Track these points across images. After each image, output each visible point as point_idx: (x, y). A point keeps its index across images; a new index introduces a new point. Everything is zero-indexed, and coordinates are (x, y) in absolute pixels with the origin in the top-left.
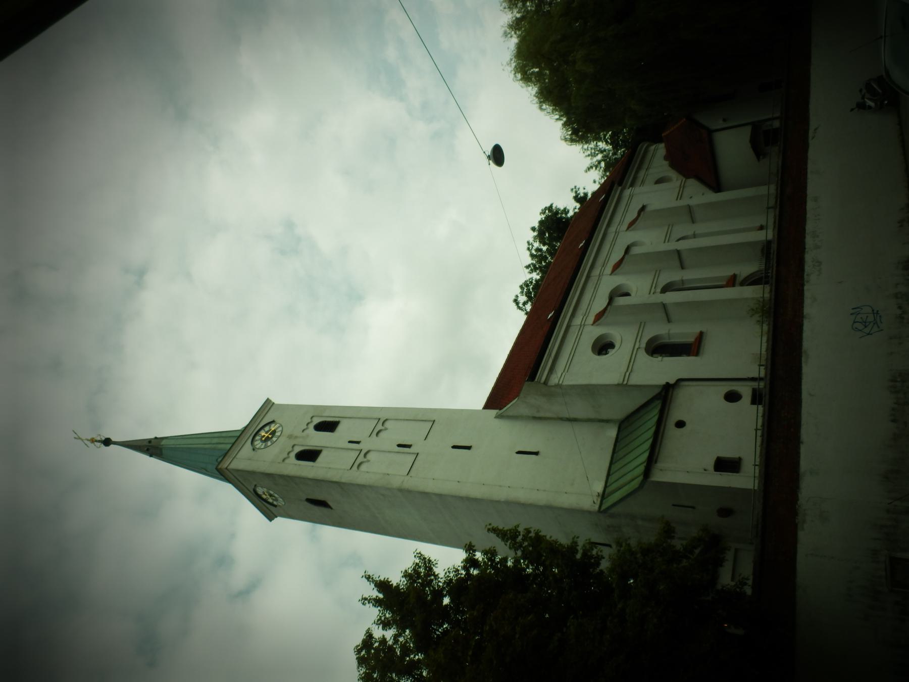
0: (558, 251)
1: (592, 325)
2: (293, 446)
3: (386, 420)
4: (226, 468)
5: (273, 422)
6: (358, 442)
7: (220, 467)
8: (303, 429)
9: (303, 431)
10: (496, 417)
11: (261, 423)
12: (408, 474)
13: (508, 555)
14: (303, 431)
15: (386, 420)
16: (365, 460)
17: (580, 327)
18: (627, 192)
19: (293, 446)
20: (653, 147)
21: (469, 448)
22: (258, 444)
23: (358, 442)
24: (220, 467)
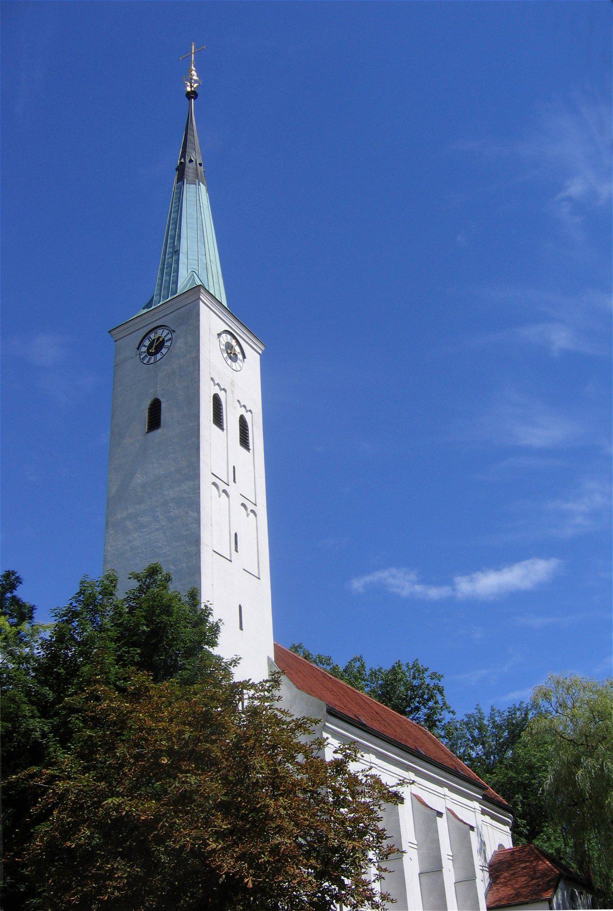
0: (562, 871)
1: (411, 793)
2: (224, 390)
3: (255, 515)
4: (200, 298)
5: (244, 357)
6: (234, 481)
7: (202, 290)
8: (240, 401)
9: (238, 401)
10: (269, 658)
11: (246, 344)
12: (214, 551)
13: (333, 759)
14: (238, 401)
15: (255, 515)
16: (221, 491)
17: (369, 762)
18: (476, 805)
19: (224, 390)
20: (507, 829)
21: (241, 628)
22: (226, 338)
23: (234, 481)
24: (202, 290)
